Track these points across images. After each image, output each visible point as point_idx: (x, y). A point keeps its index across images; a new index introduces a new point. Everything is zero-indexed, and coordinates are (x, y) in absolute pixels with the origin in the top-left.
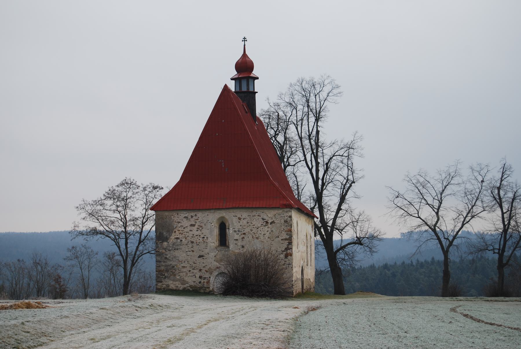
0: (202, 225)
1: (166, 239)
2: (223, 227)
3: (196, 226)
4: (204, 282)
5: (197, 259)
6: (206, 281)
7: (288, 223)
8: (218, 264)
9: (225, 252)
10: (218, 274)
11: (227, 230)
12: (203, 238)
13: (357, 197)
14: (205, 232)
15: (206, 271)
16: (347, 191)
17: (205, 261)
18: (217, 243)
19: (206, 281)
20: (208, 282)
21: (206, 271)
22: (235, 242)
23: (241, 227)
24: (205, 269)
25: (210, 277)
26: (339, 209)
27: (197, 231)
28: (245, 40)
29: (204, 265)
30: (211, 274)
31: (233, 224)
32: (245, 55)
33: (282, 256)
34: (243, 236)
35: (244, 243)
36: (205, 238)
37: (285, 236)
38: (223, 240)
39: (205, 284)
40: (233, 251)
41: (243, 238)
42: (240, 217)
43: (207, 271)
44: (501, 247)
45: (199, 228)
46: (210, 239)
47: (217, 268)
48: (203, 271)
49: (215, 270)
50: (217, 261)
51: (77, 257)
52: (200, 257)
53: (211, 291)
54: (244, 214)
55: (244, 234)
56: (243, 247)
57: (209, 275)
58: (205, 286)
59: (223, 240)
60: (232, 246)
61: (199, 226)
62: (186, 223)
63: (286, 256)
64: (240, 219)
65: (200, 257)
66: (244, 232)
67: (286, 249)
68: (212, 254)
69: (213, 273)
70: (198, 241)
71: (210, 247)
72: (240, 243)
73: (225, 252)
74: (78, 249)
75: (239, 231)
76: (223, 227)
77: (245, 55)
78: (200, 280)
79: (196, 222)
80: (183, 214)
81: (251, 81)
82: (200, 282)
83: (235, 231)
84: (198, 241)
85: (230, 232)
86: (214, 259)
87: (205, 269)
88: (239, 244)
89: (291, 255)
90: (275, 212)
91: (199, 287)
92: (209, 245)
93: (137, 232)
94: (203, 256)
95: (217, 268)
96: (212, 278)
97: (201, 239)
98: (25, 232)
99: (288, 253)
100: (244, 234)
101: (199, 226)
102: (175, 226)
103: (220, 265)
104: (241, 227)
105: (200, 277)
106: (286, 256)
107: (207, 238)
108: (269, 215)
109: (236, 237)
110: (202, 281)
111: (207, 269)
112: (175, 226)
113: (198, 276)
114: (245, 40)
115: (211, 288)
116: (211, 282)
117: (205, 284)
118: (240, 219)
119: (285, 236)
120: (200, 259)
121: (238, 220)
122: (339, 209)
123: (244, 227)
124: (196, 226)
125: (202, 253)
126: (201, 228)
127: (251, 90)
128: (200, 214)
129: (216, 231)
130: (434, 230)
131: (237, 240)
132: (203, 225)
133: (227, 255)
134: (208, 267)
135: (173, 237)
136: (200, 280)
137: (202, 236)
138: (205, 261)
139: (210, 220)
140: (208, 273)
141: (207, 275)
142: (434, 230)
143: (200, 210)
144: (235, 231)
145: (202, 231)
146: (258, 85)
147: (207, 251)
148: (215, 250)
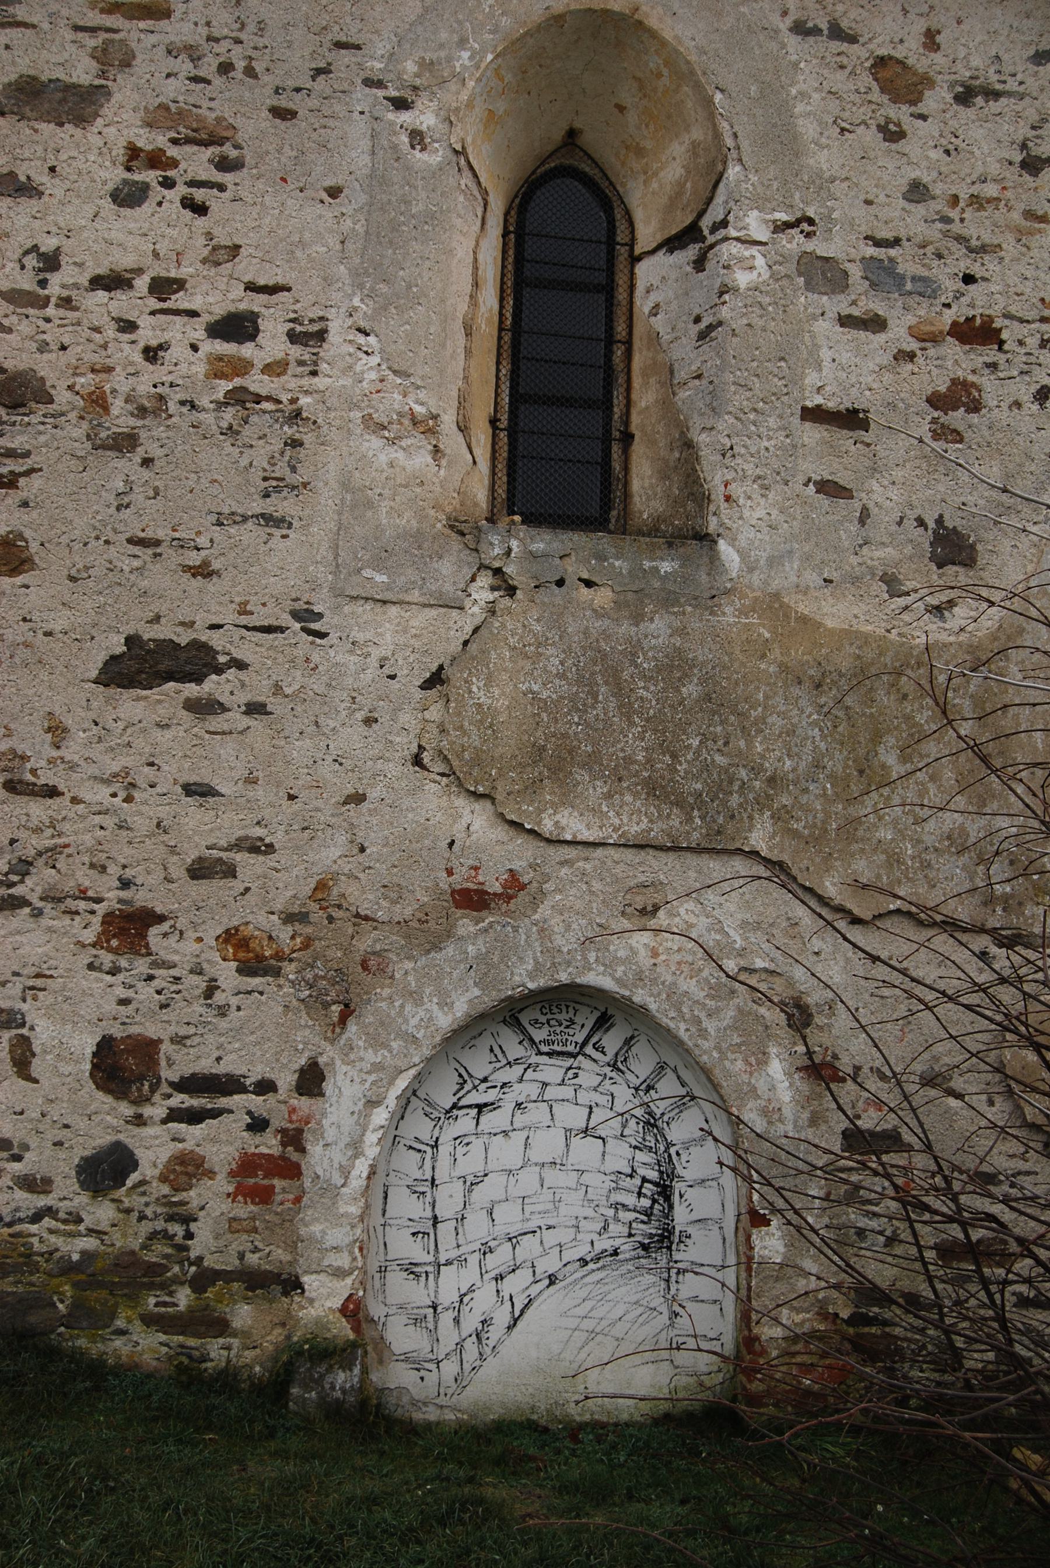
0: (219, 103)
3: (122, 122)
4: (187, 1168)
5: (77, 699)
6: (222, 1141)
8: (477, 822)
9: (633, 605)
10: (469, 1031)
11: (657, 282)
12: (237, 327)
14: (279, 228)
15: (234, 939)
17: (224, 762)
18: (466, 469)
19: (222, 1141)
20: (272, 1174)
21: (234, 939)
22: (818, 451)
23: (914, 223)
24: (220, 907)
25: (311, 1080)
26: (845, 939)
27: (129, 197)
29: (202, 829)
30: (339, 1005)
31: (784, 142)
34: (958, 361)
35: (959, 495)
36: (272, 342)
39: (213, 1199)
40: (773, 606)
41: (959, 396)
42: (911, 51)
43: (254, 961)
46: (350, 369)
47: (473, 900)
48: (186, 947)
49: (426, 934)
50: (465, 776)
52: (140, 665)
53: (324, 1353)
55: (978, 333)
56: (952, 548)
57: (307, 1039)
58: (205, 1242)
60: (754, 529)
61: (160, 116)
64: (896, 79)
65: (140, 665)
66: (978, 302)
68: (389, 638)
69: (381, 1002)
70: (131, 379)
71: (358, 500)
72: (900, 484)
73: (633, 605)
75: (882, 275)
78: (103, 1120)
79: (114, 58)
82: (107, 1170)
83: (822, 273)
84: (131, 379)
86: (410, 720)
87: (220, 907)
88: (884, 496)
91: (83, 1271)
92: (327, 464)
94: (192, 662)
95: (473, 900)
96: (344, 1088)
97: (191, 356)
100: (978, 333)
101: (160, 116)
102: (120, 1323)
103: (520, 855)
104: (914, 223)
105: (121, 1067)
107: (309, 336)
109: (843, 366)
110: (154, 1148)
111: (261, 921)
112: (120, 1323)
113: (66, 1041)
115: (323, 1299)
116: (320, 1159)
117: (213, 1199)
118: (896, 79)
120: (132, 705)
122: (845, 939)
123: (977, 227)
124: (122, 122)
125: (182, 609)
126: (196, 162)
129: (463, 262)
131: (852, 419)
132: (240, 108)
133: (675, 666)
134: (287, 880)
136: (103, 1120)
137: (214, 295)
138: (224, 762)
140: (275, 996)
141: (257, 1034)
144: (822, 273)
145: (226, 218)
147: (280, 569)
148: (449, 569)
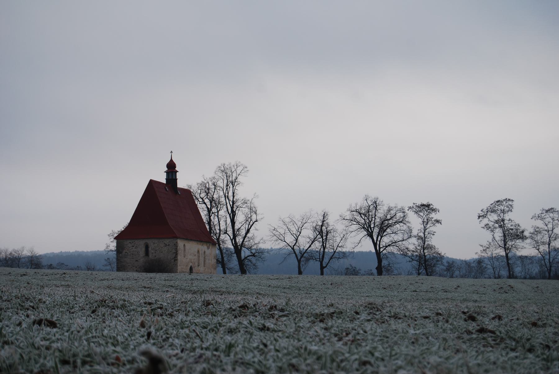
1: (121, 253)
2: (147, 247)
7: (176, 245)
13: (256, 230)
16: (251, 226)
18: (144, 255)
28: (171, 152)
32: (171, 160)
33: (173, 261)
37: (174, 251)
38: (147, 253)
44: (321, 256)
45: (137, 247)
51: (110, 264)
54: (156, 241)
59: (147, 253)
60: (150, 256)
62: (130, 245)
63: (175, 261)
67: (175, 257)
68: (142, 260)
74: (111, 259)
76: (147, 247)
77: (171, 160)
80: (129, 241)
81: (174, 173)
85: (150, 249)
89: (177, 260)
90: (170, 240)
93: (317, 251)
98: (85, 251)
99: (175, 259)
106: (175, 261)
108: (167, 241)
109: (153, 252)
114: (171, 152)
119: (174, 251)
121: (154, 244)
127: (174, 178)
128: (136, 241)
129: (144, 249)
130: (293, 249)
135: (124, 251)
139: (140, 244)
142: (293, 249)
143: (136, 239)
146: (178, 175)
